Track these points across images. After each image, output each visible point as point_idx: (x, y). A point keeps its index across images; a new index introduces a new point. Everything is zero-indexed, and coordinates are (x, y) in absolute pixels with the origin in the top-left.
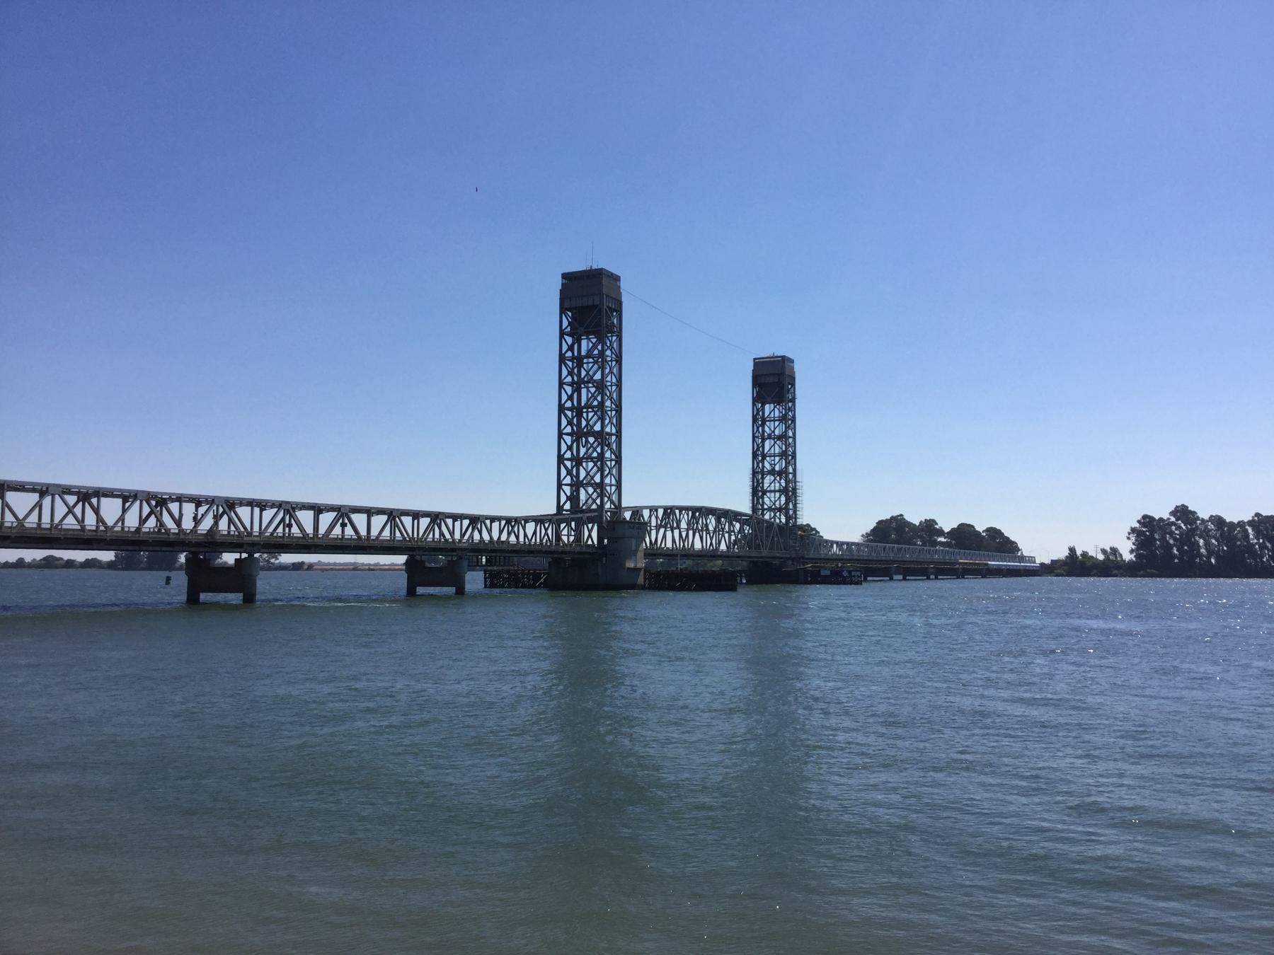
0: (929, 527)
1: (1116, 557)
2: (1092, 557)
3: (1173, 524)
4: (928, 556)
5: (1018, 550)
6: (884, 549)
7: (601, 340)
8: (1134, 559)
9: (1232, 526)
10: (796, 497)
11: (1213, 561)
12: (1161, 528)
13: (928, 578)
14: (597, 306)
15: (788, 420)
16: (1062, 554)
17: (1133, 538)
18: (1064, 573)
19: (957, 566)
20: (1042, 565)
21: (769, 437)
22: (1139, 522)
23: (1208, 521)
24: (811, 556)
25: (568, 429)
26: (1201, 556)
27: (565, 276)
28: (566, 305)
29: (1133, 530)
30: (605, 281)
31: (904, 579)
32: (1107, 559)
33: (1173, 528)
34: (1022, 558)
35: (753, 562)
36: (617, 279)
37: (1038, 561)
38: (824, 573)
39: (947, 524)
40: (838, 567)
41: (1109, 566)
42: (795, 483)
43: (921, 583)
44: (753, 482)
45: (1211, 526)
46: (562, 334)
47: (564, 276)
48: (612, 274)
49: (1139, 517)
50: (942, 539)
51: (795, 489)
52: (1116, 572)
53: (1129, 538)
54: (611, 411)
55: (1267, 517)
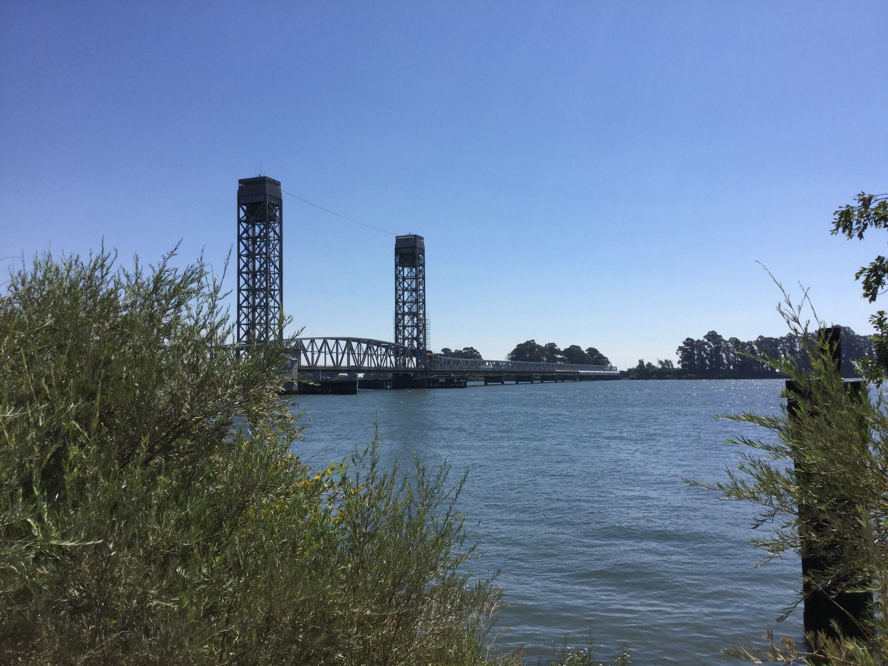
0: (551, 347)
1: (669, 366)
2: (654, 366)
3: (706, 344)
4: (552, 369)
5: (609, 362)
6: (449, 362)
7: (267, 227)
8: (680, 367)
9: (744, 345)
10: (425, 330)
11: (731, 368)
12: (697, 347)
13: (576, 381)
14: (261, 203)
15: (419, 277)
16: (634, 365)
17: (680, 353)
18: (636, 378)
19: (555, 374)
20: (622, 372)
21: (407, 290)
22: (684, 343)
23: (728, 342)
24: (438, 369)
25: (245, 287)
26: (723, 364)
27: (241, 181)
28: (242, 202)
29: (680, 348)
30: (268, 185)
31: (517, 383)
32: (663, 367)
33: (706, 346)
34: (611, 368)
35: (397, 374)
36: (278, 184)
37: (619, 370)
38: (441, 380)
39: (562, 346)
40: (451, 377)
41: (664, 372)
42: (425, 320)
43: (528, 385)
44: (396, 320)
45: (730, 345)
46: (239, 221)
47: (241, 181)
48: (274, 180)
49: (684, 340)
50: (559, 356)
51: (424, 325)
52: (669, 376)
53: (677, 354)
54: (274, 274)
55: (766, 338)
